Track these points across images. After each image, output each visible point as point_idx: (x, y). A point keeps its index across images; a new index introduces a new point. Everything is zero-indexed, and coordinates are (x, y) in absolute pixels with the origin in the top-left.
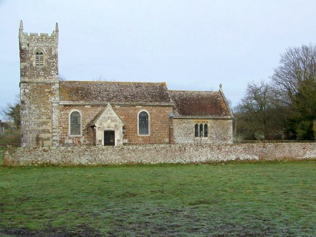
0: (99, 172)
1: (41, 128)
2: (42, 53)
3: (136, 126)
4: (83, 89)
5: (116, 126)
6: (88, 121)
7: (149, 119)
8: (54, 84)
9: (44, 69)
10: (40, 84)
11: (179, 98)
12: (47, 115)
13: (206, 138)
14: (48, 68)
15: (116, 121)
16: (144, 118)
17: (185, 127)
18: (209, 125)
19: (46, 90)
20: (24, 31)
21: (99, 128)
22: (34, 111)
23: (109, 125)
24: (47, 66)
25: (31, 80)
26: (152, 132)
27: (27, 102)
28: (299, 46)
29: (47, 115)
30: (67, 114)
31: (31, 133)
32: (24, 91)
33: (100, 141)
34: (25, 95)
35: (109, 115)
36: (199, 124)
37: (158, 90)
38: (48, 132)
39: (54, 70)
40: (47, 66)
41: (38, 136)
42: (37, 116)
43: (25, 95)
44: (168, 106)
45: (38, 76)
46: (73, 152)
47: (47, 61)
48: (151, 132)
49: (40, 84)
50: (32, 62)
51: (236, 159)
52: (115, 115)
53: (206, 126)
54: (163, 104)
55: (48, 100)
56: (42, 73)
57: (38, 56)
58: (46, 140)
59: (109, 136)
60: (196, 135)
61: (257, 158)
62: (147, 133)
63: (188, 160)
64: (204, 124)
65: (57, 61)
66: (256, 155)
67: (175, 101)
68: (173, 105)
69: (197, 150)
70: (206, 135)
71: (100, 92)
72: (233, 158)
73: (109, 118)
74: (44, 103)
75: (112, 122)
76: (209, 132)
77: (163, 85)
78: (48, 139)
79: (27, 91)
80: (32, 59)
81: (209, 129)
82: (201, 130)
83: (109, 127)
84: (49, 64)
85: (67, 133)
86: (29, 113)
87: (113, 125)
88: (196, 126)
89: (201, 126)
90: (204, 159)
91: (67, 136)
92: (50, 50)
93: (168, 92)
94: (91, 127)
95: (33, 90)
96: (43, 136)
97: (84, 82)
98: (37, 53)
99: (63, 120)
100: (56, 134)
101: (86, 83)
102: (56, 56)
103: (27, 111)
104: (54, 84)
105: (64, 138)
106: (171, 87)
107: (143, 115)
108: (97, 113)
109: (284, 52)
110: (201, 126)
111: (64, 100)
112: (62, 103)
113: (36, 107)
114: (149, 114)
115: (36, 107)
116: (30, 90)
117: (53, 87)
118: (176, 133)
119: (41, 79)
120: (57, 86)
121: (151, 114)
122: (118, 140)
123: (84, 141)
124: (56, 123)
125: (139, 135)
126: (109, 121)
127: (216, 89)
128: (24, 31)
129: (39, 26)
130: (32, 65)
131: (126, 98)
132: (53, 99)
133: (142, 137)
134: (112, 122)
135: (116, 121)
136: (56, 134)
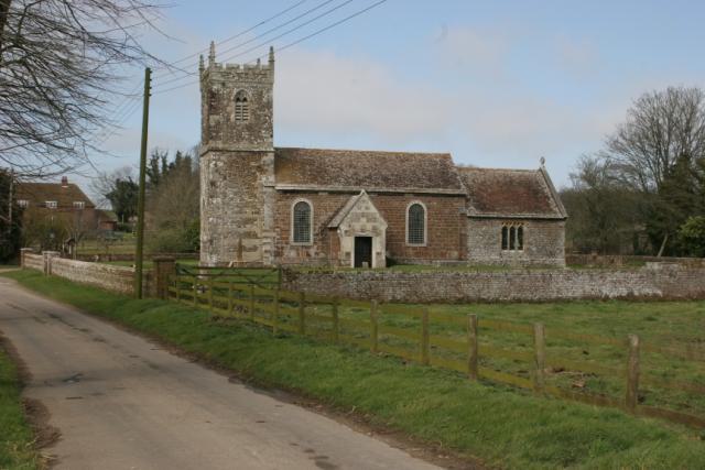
0: (553, 348)
1: (242, 230)
2: (245, 100)
3: (404, 228)
4: (311, 163)
5: (375, 229)
6: (324, 218)
7: (426, 217)
8: (265, 153)
9: (249, 128)
10: (243, 154)
11: (473, 181)
12: (254, 207)
13: (521, 251)
14: (257, 125)
15: (375, 220)
16: (416, 213)
17: (485, 233)
18: (525, 229)
19: (253, 164)
20: (216, 60)
21: (346, 232)
22: (232, 199)
23: (363, 227)
24: (253, 121)
25: (226, 146)
26: (430, 239)
27: (221, 183)
28: (662, 89)
29: (254, 207)
30: (289, 207)
31: (225, 237)
32: (216, 165)
33: (348, 254)
34: (217, 171)
35: (363, 210)
36: (509, 227)
37: (438, 167)
38: (255, 236)
39: (267, 129)
40: (253, 121)
41: (240, 242)
42: (236, 209)
43: (217, 171)
44: (459, 196)
45: (240, 138)
46: (382, 279)
47: (254, 113)
48: (428, 239)
49: (243, 154)
50: (229, 114)
51: (628, 295)
52: (373, 210)
53: (520, 230)
54: (449, 191)
55: (255, 180)
56: (245, 134)
57: (240, 104)
58: (250, 250)
59: (363, 244)
60: (504, 247)
61: (659, 292)
62: (422, 242)
63: (554, 295)
64: (517, 227)
65: (272, 114)
66: (660, 288)
67: (467, 186)
68: (465, 192)
69: (568, 279)
70: (521, 248)
71: (342, 170)
72: (624, 292)
73: (363, 215)
74: (251, 187)
75: (368, 221)
76: (525, 241)
77: (446, 157)
78: (255, 248)
79: (220, 164)
80: (229, 109)
81: (525, 236)
82: (510, 239)
83: (363, 231)
84: (257, 117)
85: (287, 238)
86: (224, 204)
87: (369, 226)
88: (505, 229)
89: (512, 230)
90: (579, 293)
91: (287, 243)
92: (260, 95)
93: (455, 170)
94: (328, 232)
95: (230, 164)
96: (246, 243)
97: (313, 151)
98: (238, 100)
99: (281, 217)
100: (269, 240)
101: (318, 151)
102: (269, 105)
103: (219, 200)
104: (265, 153)
105: (282, 248)
106: (460, 159)
107: (303, 209)
108: (339, 205)
109: (637, 97)
110: (512, 230)
111: (283, 181)
112: (280, 186)
113: (236, 194)
114: (425, 209)
115: (236, 194)
116: (225, 163)
117: (265, 158)
118: (470, 243)
119: (243, 146)
120: (271, 157)
121: (428, 208)
122: (378, 254)
123: (317, 254)
124: (269, 221)
125: (408, 245)
126: (364, 220)
127: (533, 166)
128: (216, 60)
129: (238, 53)
130: (228, 120)
131: (386, 179)
132: (264, 179)
133: (414, 248)
134: (368, 221)
135: (375, 220)
136: (269, 240)
